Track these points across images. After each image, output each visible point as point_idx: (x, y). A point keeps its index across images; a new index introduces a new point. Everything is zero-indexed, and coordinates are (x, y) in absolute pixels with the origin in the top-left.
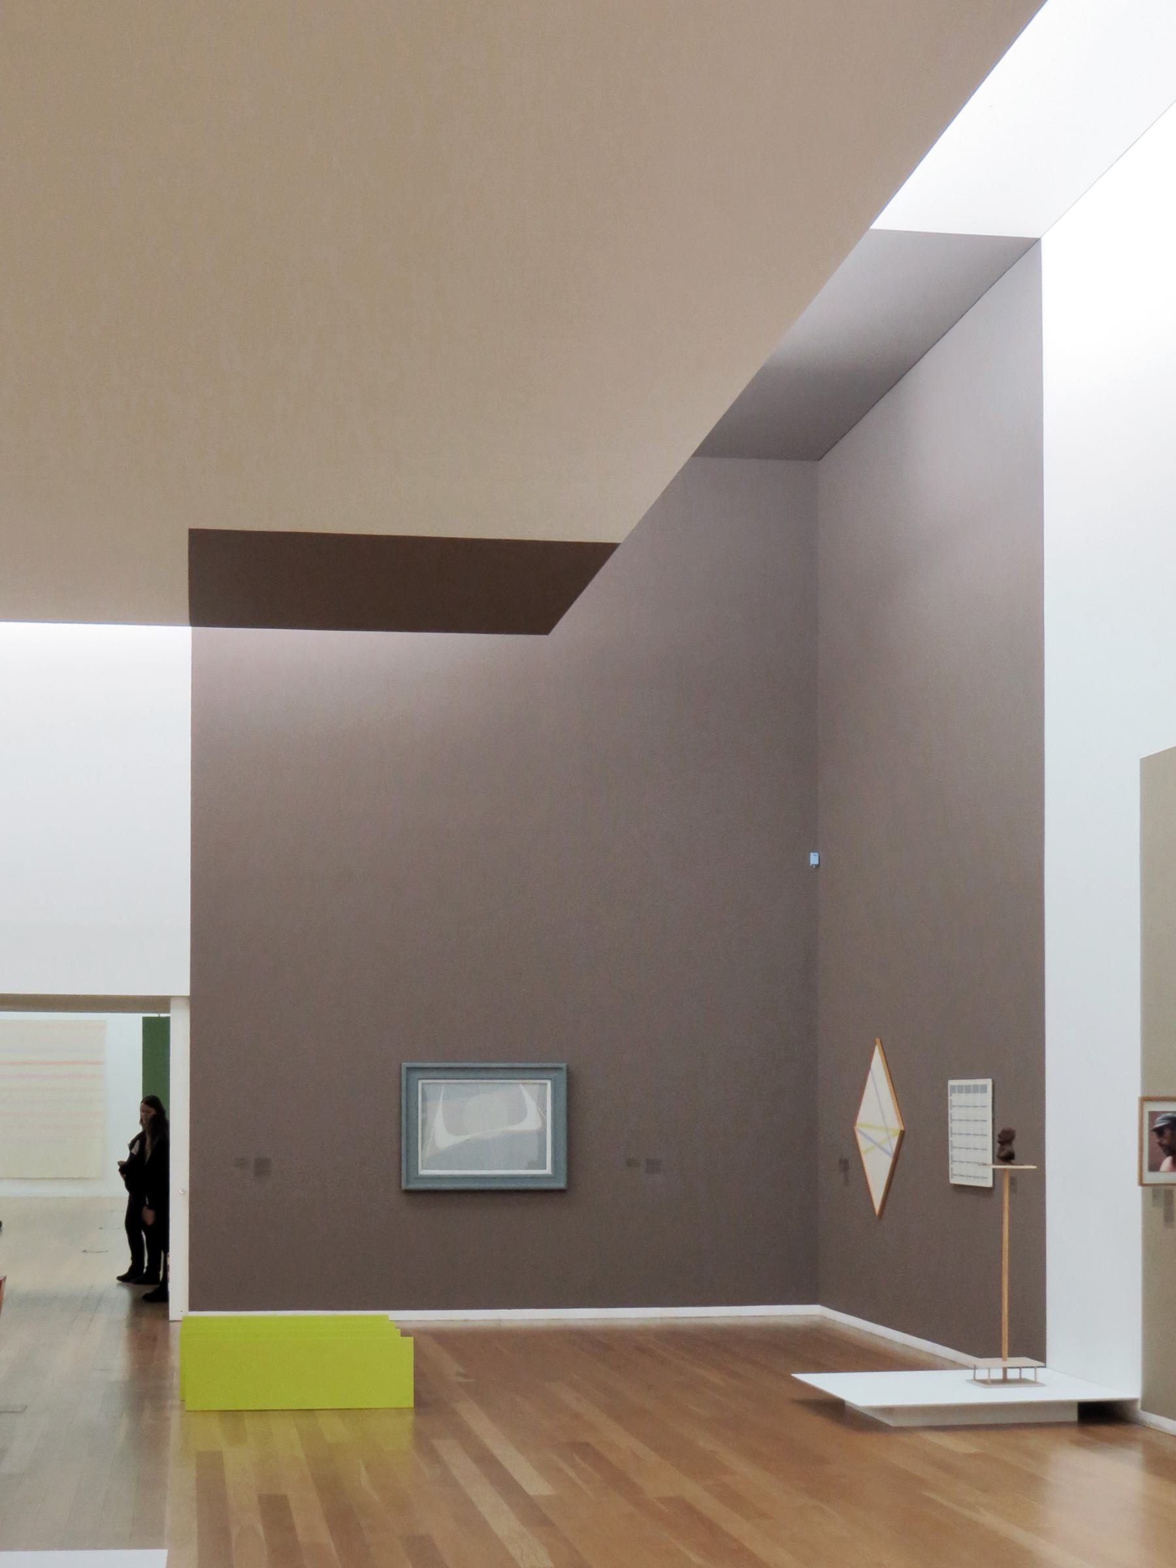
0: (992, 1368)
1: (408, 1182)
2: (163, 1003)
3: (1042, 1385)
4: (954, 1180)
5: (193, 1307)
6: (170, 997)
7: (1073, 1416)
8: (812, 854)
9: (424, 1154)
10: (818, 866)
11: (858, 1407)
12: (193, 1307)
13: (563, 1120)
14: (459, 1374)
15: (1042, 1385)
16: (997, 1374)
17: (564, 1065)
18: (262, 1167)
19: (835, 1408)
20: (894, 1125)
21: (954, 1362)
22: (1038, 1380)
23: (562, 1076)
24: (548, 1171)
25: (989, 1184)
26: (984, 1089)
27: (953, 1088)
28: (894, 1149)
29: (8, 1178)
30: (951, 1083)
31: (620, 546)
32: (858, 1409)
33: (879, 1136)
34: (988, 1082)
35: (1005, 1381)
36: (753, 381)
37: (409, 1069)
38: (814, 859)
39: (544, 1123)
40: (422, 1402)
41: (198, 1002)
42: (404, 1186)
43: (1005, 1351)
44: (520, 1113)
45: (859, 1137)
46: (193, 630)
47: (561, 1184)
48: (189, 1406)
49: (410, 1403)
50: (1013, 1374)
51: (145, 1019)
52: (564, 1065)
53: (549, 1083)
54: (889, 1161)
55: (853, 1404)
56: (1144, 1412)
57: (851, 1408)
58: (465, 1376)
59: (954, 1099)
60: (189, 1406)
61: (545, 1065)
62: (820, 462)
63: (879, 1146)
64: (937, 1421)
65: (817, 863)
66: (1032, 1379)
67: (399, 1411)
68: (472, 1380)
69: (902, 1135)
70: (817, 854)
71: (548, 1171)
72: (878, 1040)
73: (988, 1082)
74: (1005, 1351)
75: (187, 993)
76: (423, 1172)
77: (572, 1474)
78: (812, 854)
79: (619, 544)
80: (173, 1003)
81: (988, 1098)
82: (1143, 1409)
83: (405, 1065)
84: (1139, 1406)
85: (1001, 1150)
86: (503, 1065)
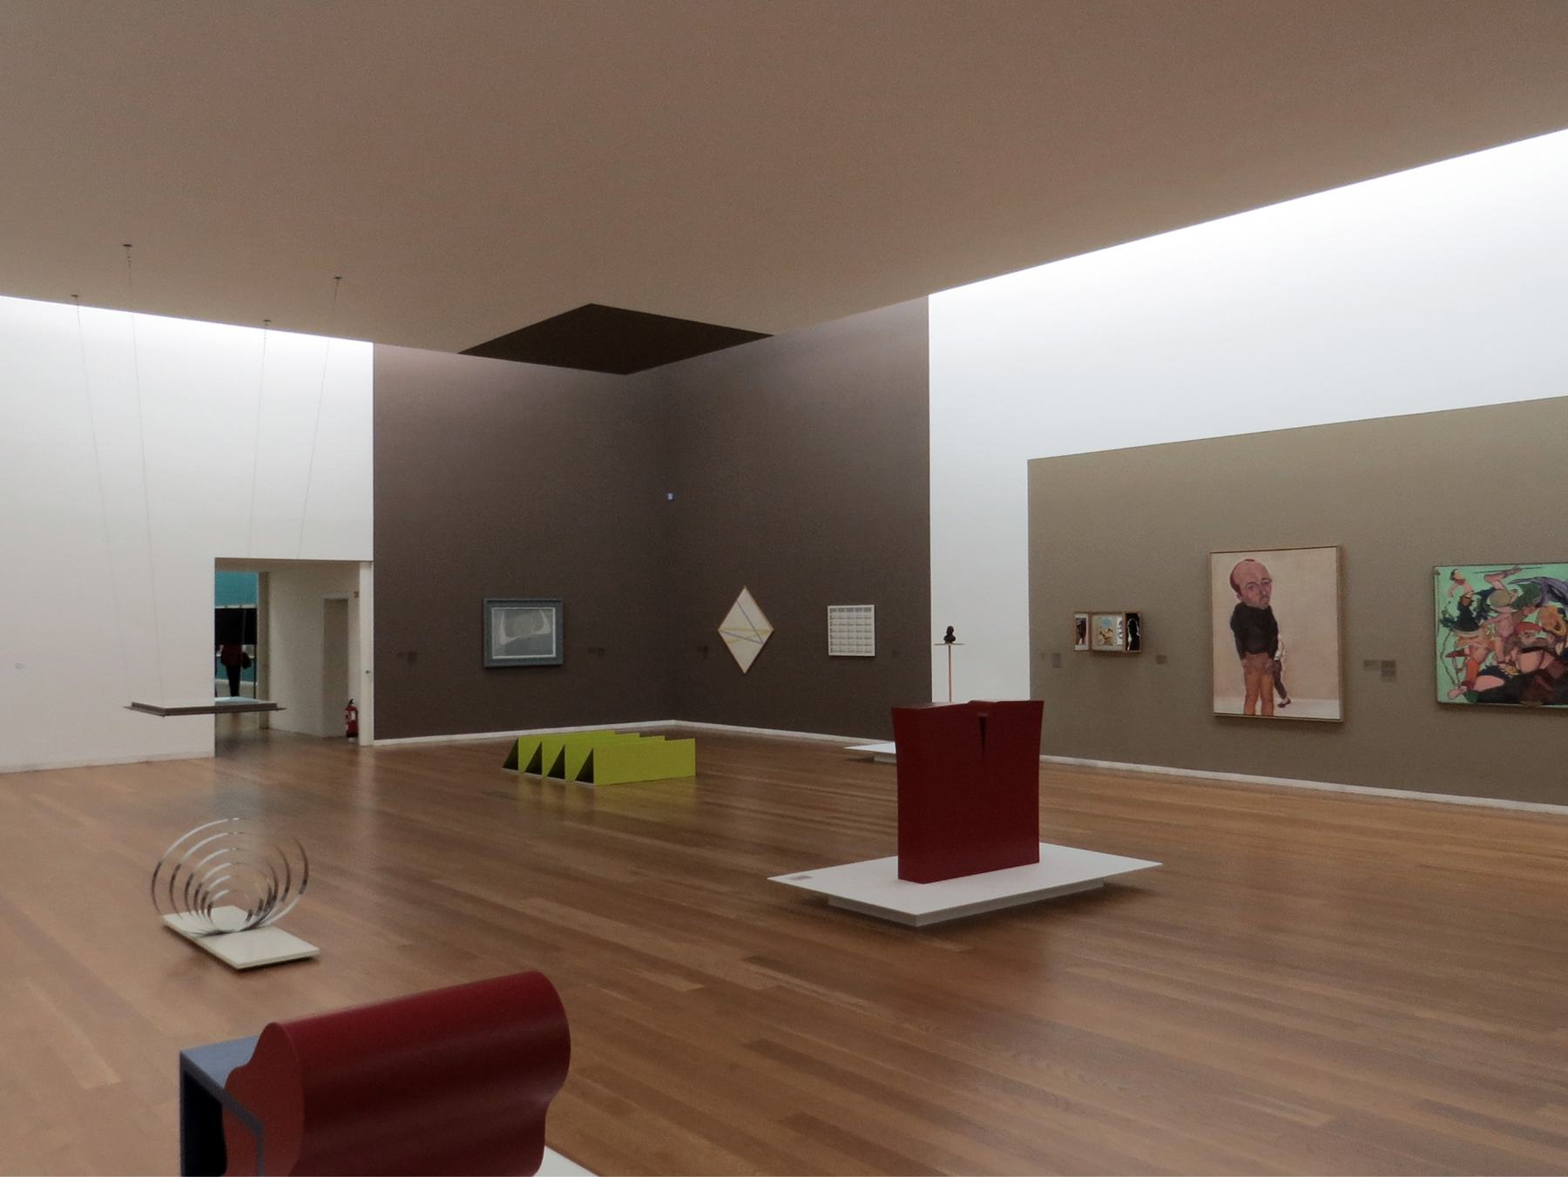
4: (830, 654)
5: (378, 735)
9: (494, 647)
12: (378, 735)
18: (412, 657)
21: (147, 762)
24: (554, 655)
25: (873, 654)
26: (870, 610)
30: (829, 607)
34: (872, 606)
37: (489, 602)
39: (552, 630)
41: (381, 564)
42: (486, 665)
44: (540, 626)
45: (722, 635)
46: (374, 347)
47: (560, 662)
49: (694, 774)
53: (554, 610)
54: (760, 646)
71: (554, 655)
73: (872, 606)
76: (495, 657)
83: (486, 600)
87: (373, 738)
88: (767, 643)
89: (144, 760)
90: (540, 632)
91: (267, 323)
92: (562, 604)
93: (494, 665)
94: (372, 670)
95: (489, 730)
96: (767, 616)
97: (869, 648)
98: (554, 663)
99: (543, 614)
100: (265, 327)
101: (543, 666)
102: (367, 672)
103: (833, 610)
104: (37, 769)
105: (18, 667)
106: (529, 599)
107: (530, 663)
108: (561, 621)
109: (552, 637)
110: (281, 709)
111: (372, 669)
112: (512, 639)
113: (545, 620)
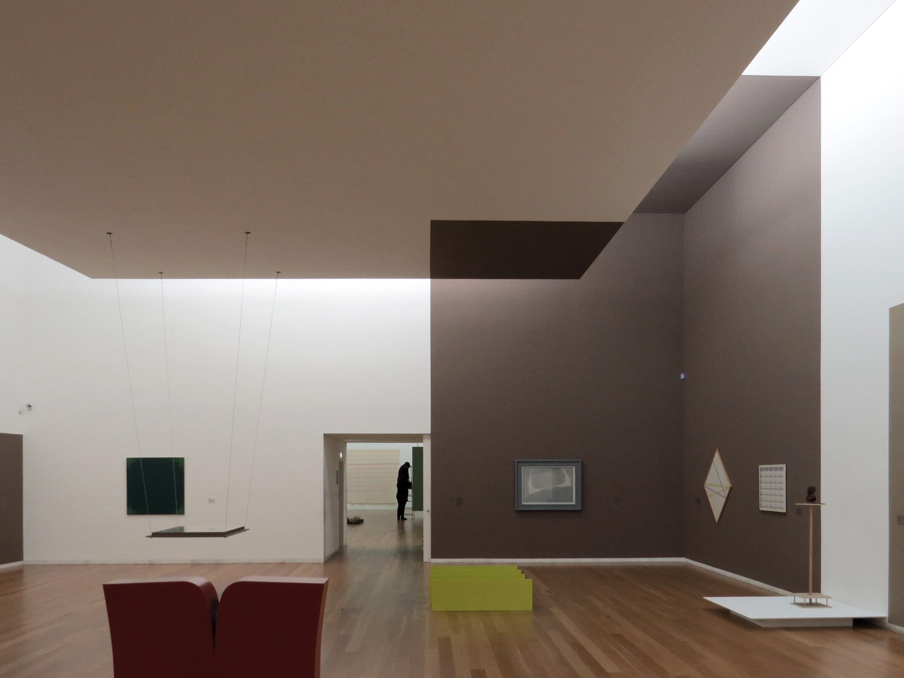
0: (800, 598)
1: (517, 507)
2: (418, 438)
3: (830, 607)
4: (761, 509)
5: (433, 557)
6: (423, 434)
7: (851, 624)
8: (681, 374)
9: (524, 495)
10: (684, 379)
11: (749, 619)
12: (433, 557)
13: (580, 481)
14: (546, 591)
15: (830, 607)
16: (808, 601)
17: (580, 460)
19: (725, 614)
20: (726, 484)
21: (282, 563)
22: (828, 605)
23: (579, 465)
24: (574, 503)
25: (784, 511)
26: (781, 469)
27: (762, 469)
28: (726, 495)
29: (368, 504)
30: (760, 466)
31: (624, 225)
32: (749, 620)
33: (718, 489)
34: (784, 466)
35: (811, 605)
36: (669, 168)
37: (518, 462)
38: (682, 376)
39: (572, 483)
40: (537, 607)
41: (435, 436)
42: (516, 509)
43: (811, 588)
44: (562, 480)
45: (706, 489)
46: (431, 281)
47: (579, 508)
48: (434, 609)
49: (530, 608)
50: (814, 601)
51: (414, 448)
52: (580, 460)
53: (574, 468)
54: (724, 500)
55: (734, 612)
56: (890, 624)
57: (732, 612)
58: (549, 592)
59: (762, 473)
60: (434, 609)
61: (563, 460)
62: (686, 214)
63: (718, 493)
64: (786, 626)
65: (683, 378)
66: (826, 604)
67: (527, 612)
68: (553, 594)
69: (731, 489)
70: (684, 374)
71: (574, 503)
72: (717, 449)
73: (784, 466)
74: (811, 588)
75: (430, 433)
77: (622, 656)
78: (681, 374)
79: (623, 223)
80: (424, 437)
81: (784, 473)
82: (889, 621)
83: (516, 460)
84: (887, 621)
85: (808, 496)
86: (567, 460)
87: (430, 557)
88: (729, 495)
89: (281, 562)
90: (562, 485)
91: (278, 274)
92: (580, 463)
93: (525, 509)
94: (430, 510)
95: (537, 557)
96: (730, 478)
97: (778, 505)
98: (573, 508)
99: (564, 470)
100: (277, 278)
101: (562, 511)
102: (428, 511)
103: (762, 469)
104: (31, 564)
105: (211, 501)
106: (569, 460)
107: (537, 509)
108: (580, 475)
109: (573, 488)
110: (247, 530)
111: (430, 509)
112: (539, 490)
113: (567, 477)
